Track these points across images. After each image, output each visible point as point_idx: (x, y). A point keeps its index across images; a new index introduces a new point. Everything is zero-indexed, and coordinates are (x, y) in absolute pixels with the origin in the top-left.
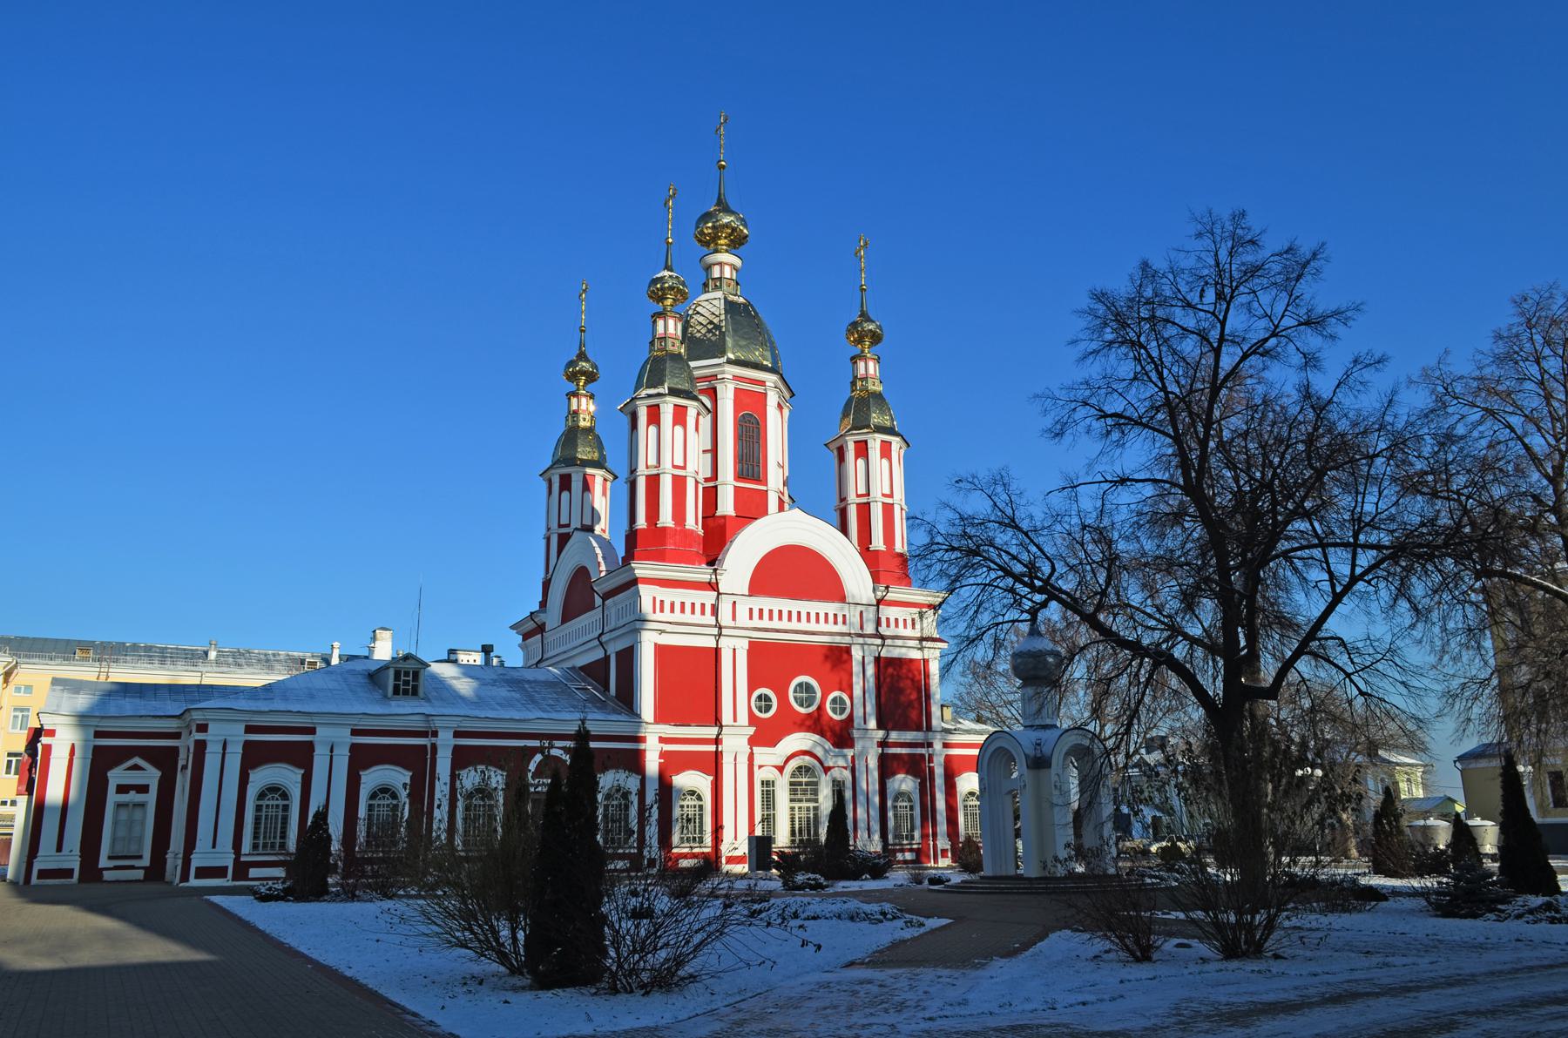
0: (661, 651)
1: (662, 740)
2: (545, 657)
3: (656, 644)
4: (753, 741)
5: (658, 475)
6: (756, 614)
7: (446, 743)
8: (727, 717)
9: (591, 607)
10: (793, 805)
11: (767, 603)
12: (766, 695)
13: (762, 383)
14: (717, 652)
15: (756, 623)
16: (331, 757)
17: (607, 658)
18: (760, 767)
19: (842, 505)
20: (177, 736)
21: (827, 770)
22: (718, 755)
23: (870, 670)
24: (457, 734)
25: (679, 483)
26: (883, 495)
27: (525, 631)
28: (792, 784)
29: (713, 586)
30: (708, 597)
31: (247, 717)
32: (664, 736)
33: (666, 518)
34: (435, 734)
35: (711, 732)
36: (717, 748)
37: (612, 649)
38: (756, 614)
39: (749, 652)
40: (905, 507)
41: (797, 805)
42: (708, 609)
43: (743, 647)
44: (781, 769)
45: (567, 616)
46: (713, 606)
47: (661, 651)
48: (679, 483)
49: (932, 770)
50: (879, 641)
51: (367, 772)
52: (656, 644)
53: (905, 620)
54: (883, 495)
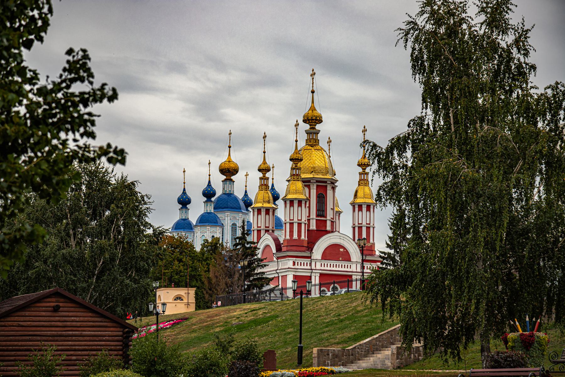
11: (326, 262)
15: (323, 268)
17: (279, 277)
23: (329, 262)
25: (300, 225)
29: (310, 257)
30: (308, 261)
31: (320, 271)
33: (295, 236)
48: (300, 225)
50: (311, 271)
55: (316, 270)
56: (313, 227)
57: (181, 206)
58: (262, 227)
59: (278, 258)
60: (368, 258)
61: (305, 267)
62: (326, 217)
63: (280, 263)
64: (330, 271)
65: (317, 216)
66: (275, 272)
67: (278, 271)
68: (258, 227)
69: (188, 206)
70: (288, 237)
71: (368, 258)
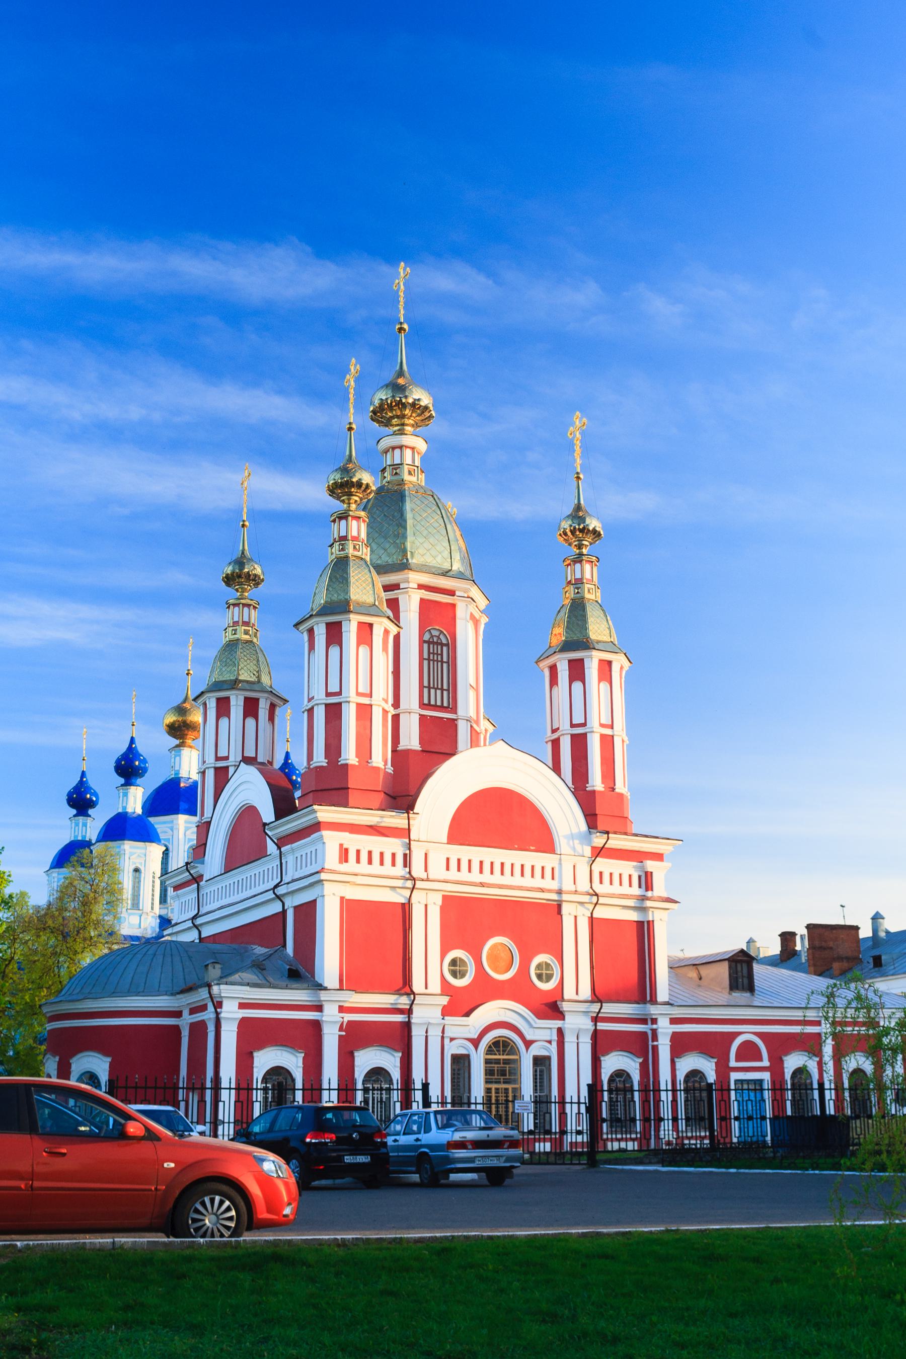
0: (349, 907)
1: (674, 1021)
2: (203, 911)
3: (342, 898)
4: (447, 1011)
5: (340, 704)
6: (453, 864)
7: (665, 1029)
8: (417, 984)
9: (261, 853)
10: (489, 1086)
12: (461, 960)
13: (452, 593)
14: (406, 909)
15: (453, 874)
16: (578, 1043)
17: (284, 912)
18: (452, 1039)
19: (555, 736)
20: (178, 1014)
21: (528, 1044)
22: (407, 1027)
24: (342, 1009)
26: (602, 725)
27: (175, 884)
28: (487, 1062)
30: (394, 845)
32: (346, 1005)
34: (654, 1021)
35: (404, 1002)
36: (596, 1025)
37: (291, 903)
38: (453, 864)
39: (442, 908)
40: (626, 739)
41: (494, 1086)
42: (400, 860)
43: (435, 902)
44: (476, 1042)
45: (232, 863)
46: (405, 855)
47: (349, 907)
49: (655, 1049)
50: (409, 884)
51: (681, 1060)
52: (342, 898)
53: (394, 855)
54: (602, 725)
55: (428, 880)
56: (411, 739)
57: (74, 812)
58: (231, 758)
59: (281, 843)
60: (617, 842)
61: (387, 869)
62: (454, 710)
63: (289, 860)
64: (482, 885)
65: (422, 705)
66: (270, 895)
67: (199, 921)
68: (218, 759)
69: (90, 812)
70: (320, 759)
71: (617, 842)
